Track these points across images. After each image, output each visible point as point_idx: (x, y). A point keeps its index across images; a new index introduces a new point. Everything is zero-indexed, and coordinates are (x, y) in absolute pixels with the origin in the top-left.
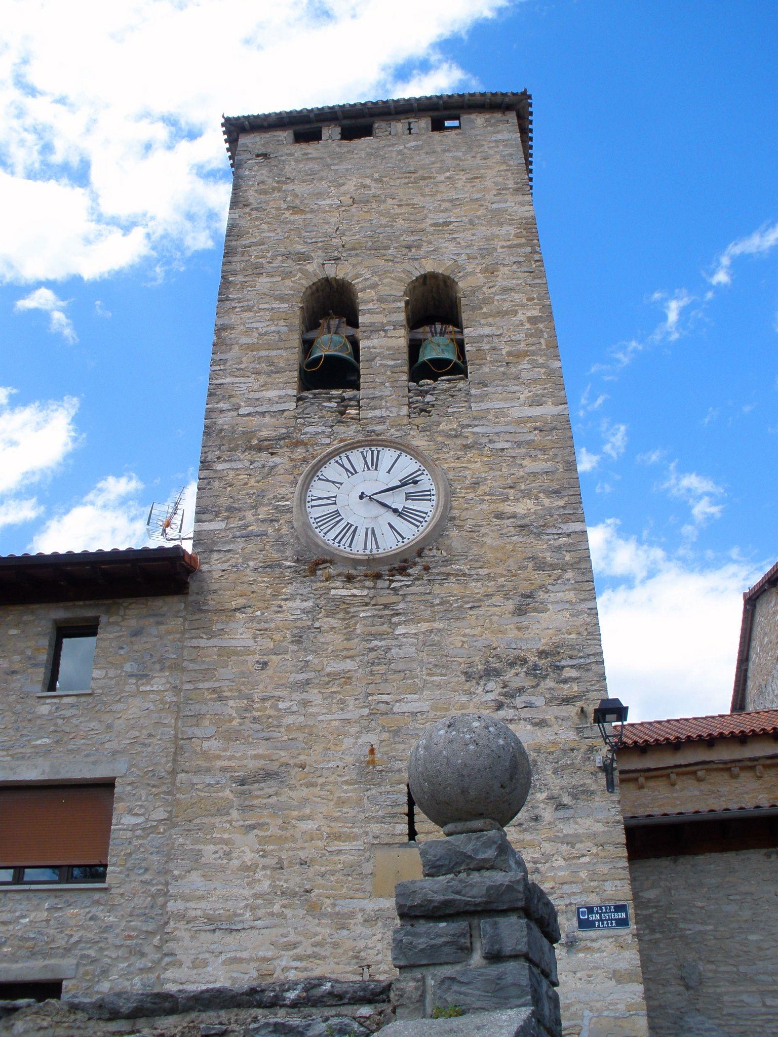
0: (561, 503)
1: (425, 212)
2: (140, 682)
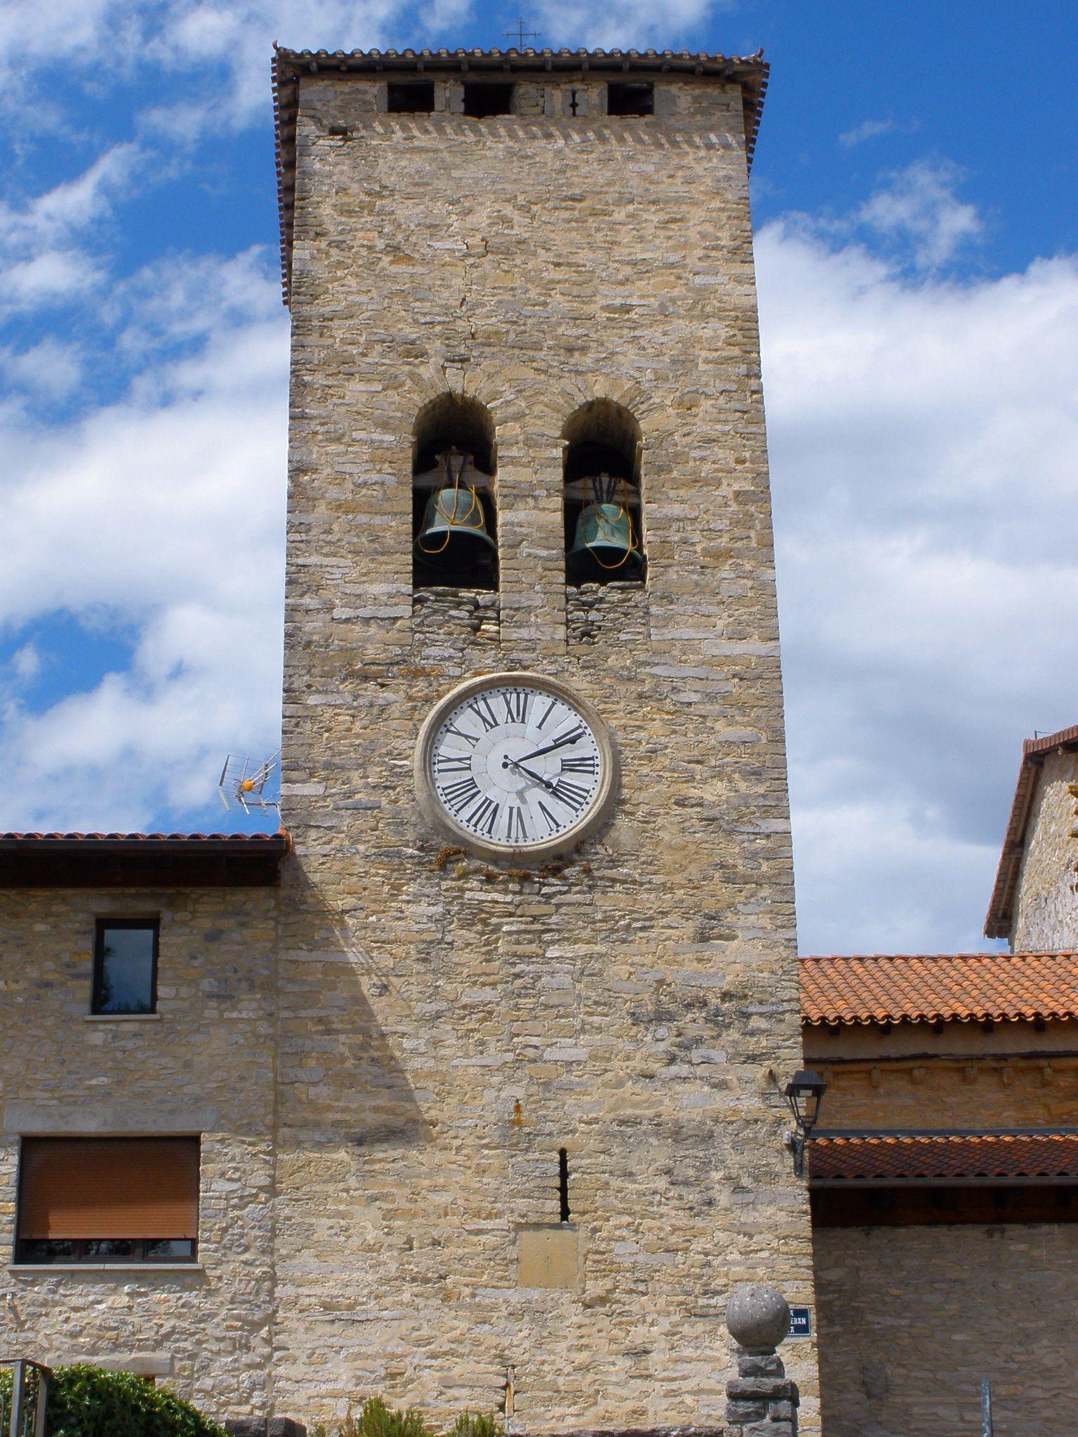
0: (761, 789)
1: (596, 281)
2: (223, 1006)
